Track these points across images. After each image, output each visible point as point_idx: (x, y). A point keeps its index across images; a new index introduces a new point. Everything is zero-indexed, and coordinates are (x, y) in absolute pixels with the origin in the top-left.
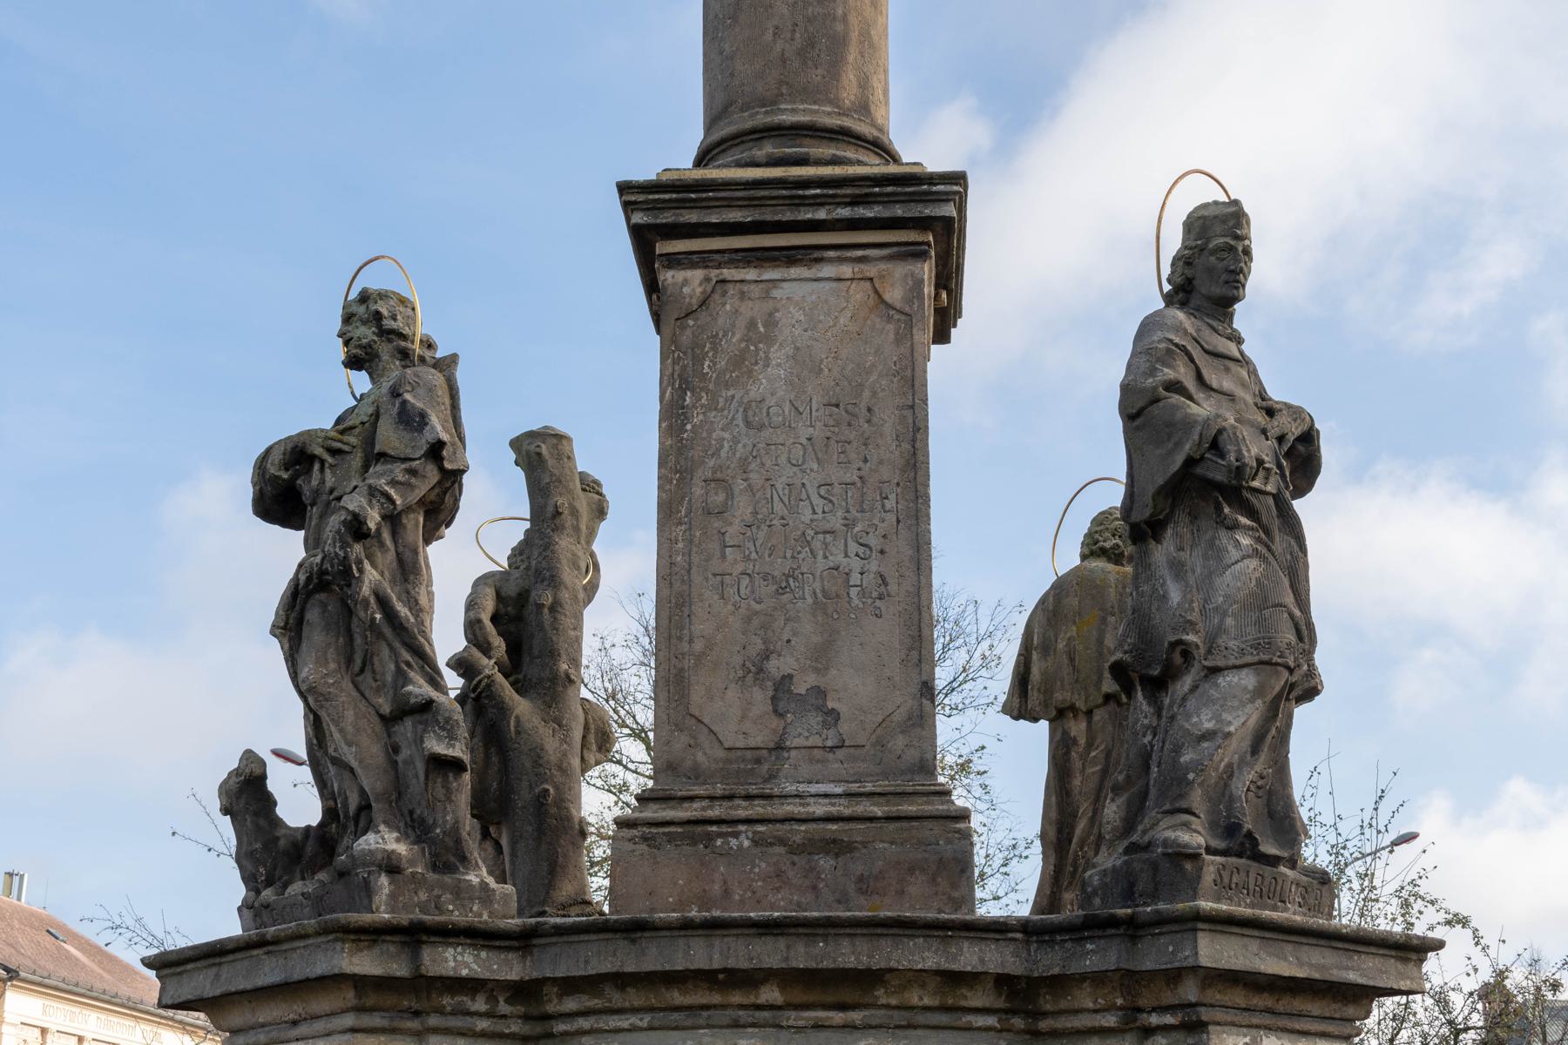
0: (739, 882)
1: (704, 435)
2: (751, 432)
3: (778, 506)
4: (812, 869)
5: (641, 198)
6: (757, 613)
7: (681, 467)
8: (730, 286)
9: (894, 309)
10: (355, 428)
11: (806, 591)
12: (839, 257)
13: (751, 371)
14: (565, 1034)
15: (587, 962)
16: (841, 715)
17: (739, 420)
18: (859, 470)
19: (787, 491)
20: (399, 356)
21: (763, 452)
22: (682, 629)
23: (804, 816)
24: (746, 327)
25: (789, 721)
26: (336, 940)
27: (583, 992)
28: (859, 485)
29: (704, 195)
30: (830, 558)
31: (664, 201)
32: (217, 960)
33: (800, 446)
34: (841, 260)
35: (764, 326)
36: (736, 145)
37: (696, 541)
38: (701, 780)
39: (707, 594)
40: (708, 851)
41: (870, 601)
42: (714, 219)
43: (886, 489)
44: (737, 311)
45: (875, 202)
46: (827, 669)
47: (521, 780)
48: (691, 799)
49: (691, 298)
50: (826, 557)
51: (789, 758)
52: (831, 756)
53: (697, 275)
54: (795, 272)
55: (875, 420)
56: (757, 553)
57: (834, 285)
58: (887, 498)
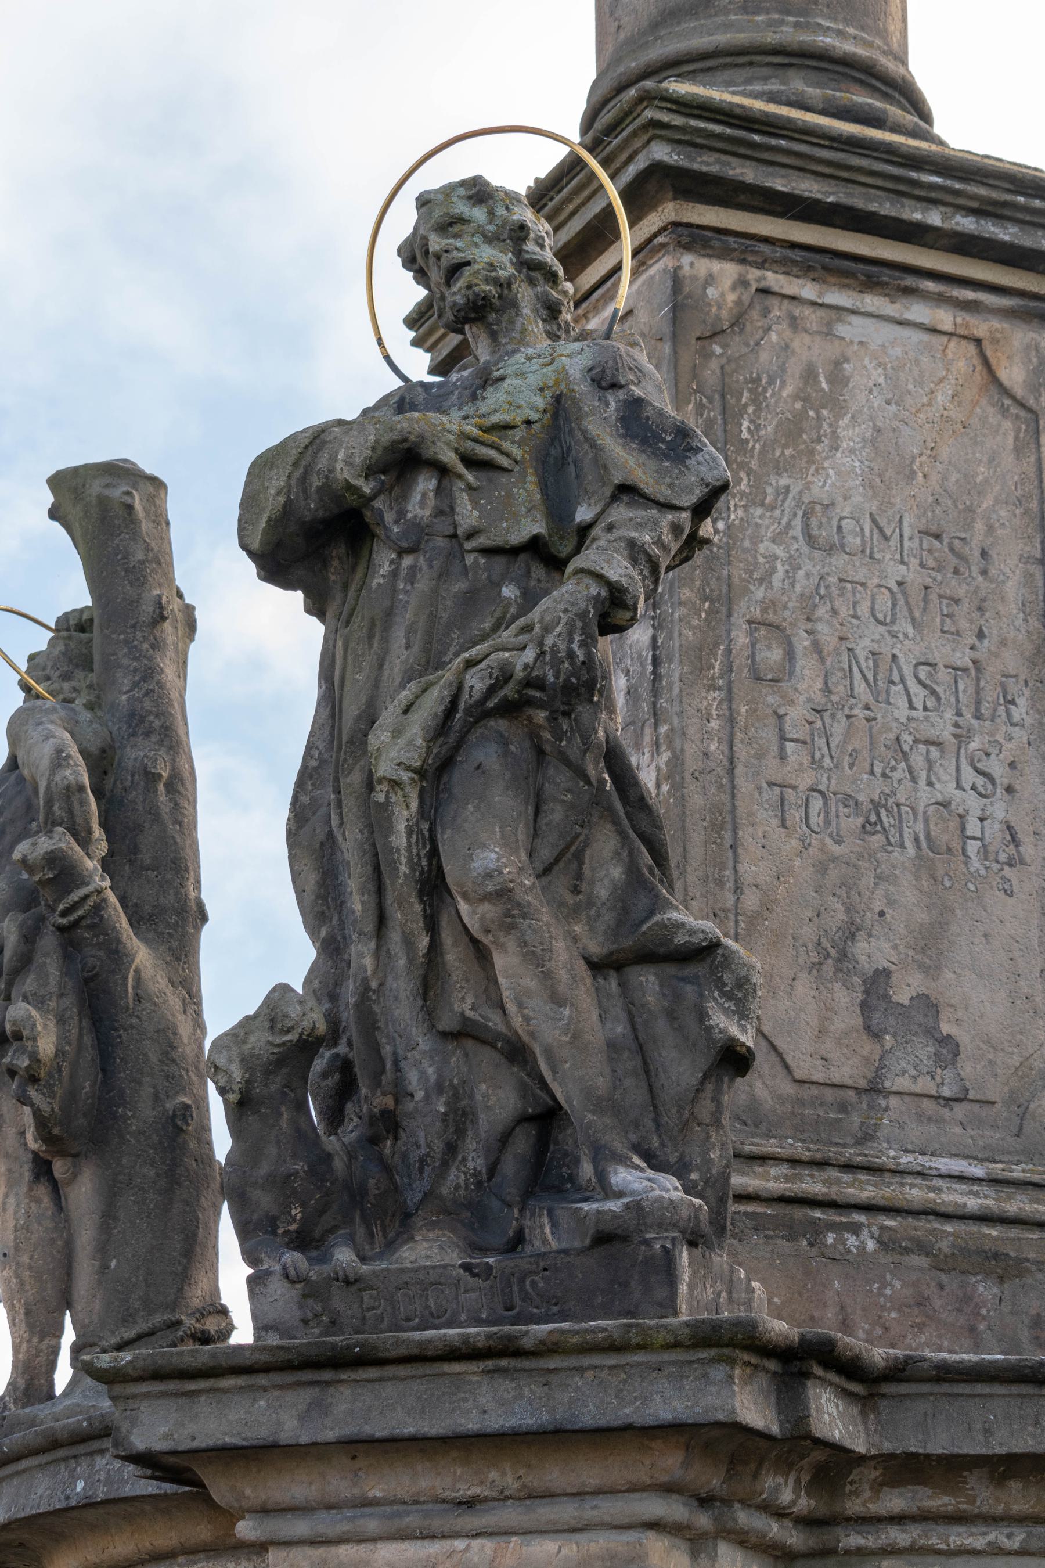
0: (864, 1310)
1: (747, 544)
2: (817, 554)
3: (860, 687)
4: (967, 1299)
5: (678, 120)
6: (834, 859)
7: (712, 590)
8: (774, 301)
9: (1013, 397)
10: (514, 427)
11: (906, 835)
12: (940, 294)
13: (812, 452)
14: (860, 1552)
15: (987, 1432)
16: (962, 1049)
17: (797, 531)
18: (972, 648)
19: (871, 662)
20: (544, 313)
21: (835, 591)
22: (722, 867)
23: (950, 1209)
24: (802, 377)
25: (888, 1047)
26: (719, 1360)
27: (924, 1483)
28: (973, 672)
29: (774, 142)
30: (938, 786)
31: (712, 135)
32: (327, 1375)
33: (886, 592)
34: (941, 299)
35: (828, 382)
36: (737, 65)
37: (741, 720)
38: (763, 1127)
39: (762, 815)
40: (815, 1251)
41: (996, 867)
42: (779, 184)
43: (1013, 687)
44: (787, 346)
45: (1010, 219)
46: (938, 968)
47: (140, 1083)
48: (762, 1159)
49: (719, 308)
50: (930, 784)
51: (887, 1109)
52: (946, 1112)
53: (727, 271)
54: (872, 302)
55: (993, 572)
56: (832, 757)
57: (925, 337)
58: (1013, 702)
